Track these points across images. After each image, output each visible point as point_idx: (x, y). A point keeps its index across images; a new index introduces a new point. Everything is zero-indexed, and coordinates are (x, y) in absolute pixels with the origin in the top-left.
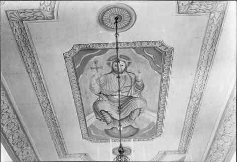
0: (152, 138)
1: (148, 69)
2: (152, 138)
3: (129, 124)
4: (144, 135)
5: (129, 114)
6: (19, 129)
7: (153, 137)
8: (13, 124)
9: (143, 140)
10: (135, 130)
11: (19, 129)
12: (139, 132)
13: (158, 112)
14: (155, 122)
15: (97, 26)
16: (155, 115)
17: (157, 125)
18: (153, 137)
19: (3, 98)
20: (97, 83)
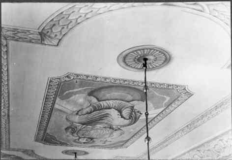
0: (68, 77)
1: (145, 141)
2: (68, 77)
3: (101, 103)
4: (81, 85)
5: (95, 112)
6: (221, 140)
7: (67, 79)
8: (195, 156)
9: (87, 76)
10: (95, 94)
11: (221, 140)
12: (90, 91)
13: (52, 110)
14: (58, 100)
15: (145, 154)
16: (56, 106)
17: (56, 95)
18: (67, 79)
19: (186, 157)
20: (50, 133)
